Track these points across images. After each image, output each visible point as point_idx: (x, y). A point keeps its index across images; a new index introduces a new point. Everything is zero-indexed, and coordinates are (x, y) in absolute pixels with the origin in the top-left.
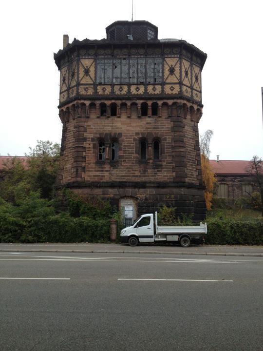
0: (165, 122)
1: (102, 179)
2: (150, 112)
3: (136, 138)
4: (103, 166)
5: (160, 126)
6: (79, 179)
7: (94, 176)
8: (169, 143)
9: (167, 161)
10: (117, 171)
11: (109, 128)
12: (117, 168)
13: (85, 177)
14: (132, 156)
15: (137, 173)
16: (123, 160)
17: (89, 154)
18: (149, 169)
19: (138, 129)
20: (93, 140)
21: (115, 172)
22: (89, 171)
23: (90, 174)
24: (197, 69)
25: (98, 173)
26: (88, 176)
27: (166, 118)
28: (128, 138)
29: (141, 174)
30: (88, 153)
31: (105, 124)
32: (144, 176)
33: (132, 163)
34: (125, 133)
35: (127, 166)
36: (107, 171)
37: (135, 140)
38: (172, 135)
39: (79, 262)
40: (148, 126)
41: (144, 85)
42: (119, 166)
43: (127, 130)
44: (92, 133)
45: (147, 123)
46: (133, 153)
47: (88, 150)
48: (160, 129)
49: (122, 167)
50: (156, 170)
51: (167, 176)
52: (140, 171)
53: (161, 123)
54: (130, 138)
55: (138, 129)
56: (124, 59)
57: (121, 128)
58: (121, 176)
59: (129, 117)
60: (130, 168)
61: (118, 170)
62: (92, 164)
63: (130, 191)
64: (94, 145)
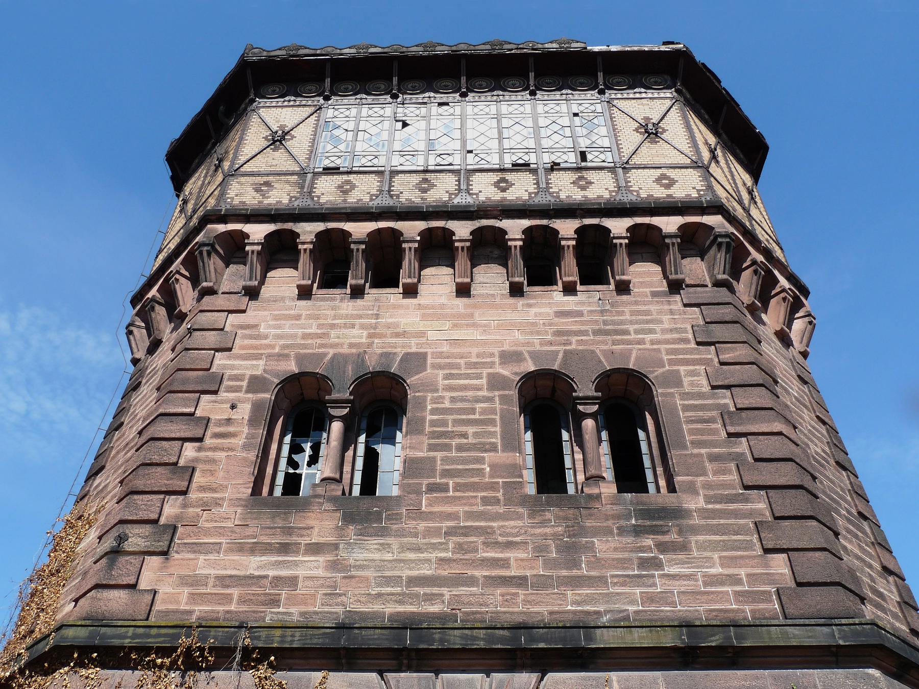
0: (653, 308)
2: (569, 269)
3: (505, 373)
4: (295, 520)
6: (115, 601)
7: (224, 581)
9: (708, 486)
10: (385, 547)
11: (358, 335)
12: (383, 532)
13: (164, 590)
14: (481, 460)
15: (519, 561)
16: (425, 482)
17: (223, 455)
18: (596, 532)
19: (518, 336)
20: (256, 384)
21: (368, 553)
22: (197, 548)
23: (205, 566)
25: (253, 564)
26: (184, 581)
28: (459, 377)
29: (548, 564)
30: (215, 449)
31: (335, 317)
32: (577, 582)
33: (486, 501)
34: (440, 355)
36: (315, 549)
37: (496, 382)
40: (568, 324)
41: (534, 171)
43: (454, 342)
44: (257, 357)
46: (493, 448)
47: (217, 436)
48: (633, 336)
49: (422, 525)
50: (649, 541)
52: (540, 550)
54: (468, 376)
55: (518, 336)
57: (422, 334)
58: (413, 581)
59: (463, 291)
60: (467, 531)
61: (389, 540)
62: (225, 509)
64: (257, 407)
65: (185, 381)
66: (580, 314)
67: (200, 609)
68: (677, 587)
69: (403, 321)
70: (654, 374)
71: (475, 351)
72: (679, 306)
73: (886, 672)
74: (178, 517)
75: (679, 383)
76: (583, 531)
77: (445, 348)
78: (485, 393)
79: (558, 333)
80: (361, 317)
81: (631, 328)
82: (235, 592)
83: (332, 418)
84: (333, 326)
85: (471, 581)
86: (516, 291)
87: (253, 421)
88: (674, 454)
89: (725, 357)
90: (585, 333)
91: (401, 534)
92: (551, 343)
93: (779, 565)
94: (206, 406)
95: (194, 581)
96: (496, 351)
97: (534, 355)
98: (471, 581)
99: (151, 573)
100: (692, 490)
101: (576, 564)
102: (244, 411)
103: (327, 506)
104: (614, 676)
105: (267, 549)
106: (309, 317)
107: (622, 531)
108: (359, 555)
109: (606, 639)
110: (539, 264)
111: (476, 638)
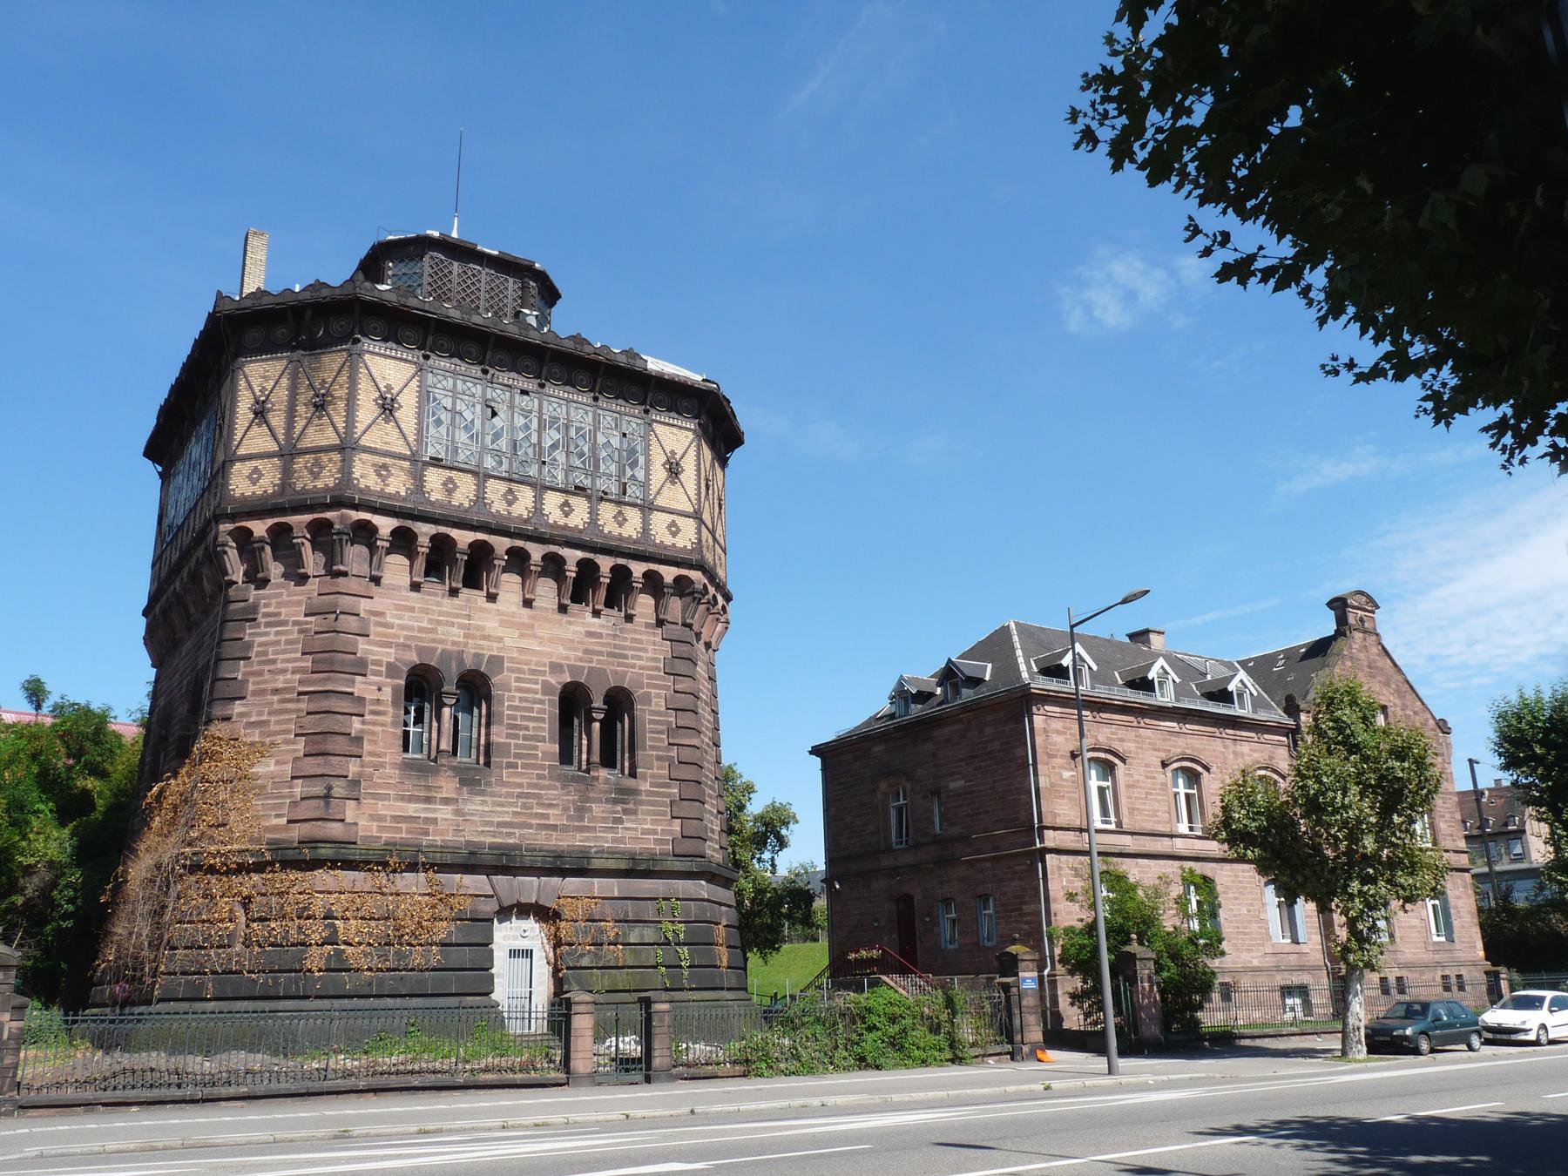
1: (427, 833)
5: (631, 649)
7: (396, 819)
8: (658, 713)
9: (653, 776)
12: (482, 793)
14: (536, 748)
15: (555, 816)
17: (379, 729)
19: (562, 650)
20: (392, 670)
21: (476, 805)
25: (412, 809)
26: (373, 818)
27: (648, 625)
29: (570, 818)
30: (374, 724)
32: (582, 829)
33: (539, 777)
34: (512, 660)
35: (520, 785)
36: (446, 801)
38: (666, 688)
39: (1394, 1078)
41: (589, 498)
42: (489, 784)
43: (522, 650)
44: (389, 645)
45: (590, 634)
50: (619, 808)
51: (655, 832)
52: (566, 809)
54: (530, 681)
55: (562, 650)
56: (524, 392)
57: (500, 639)
58: (500, 824)
60: (528, 795)
63: (531, 888)
64: (395, 689)
65: (343, 663)
66: (599, 636)
67: (386, 836)
68: (628, 834)
69: (487, 624)
70: (637, 693)
71: (535, 659)
72: (658, 639)
73: (708, 881)
74: (360, 774)
75: (649, 704)
76: (588, 800)
77: (515, 655)
78: (539, 696)
79: (587, 652)
80: (457, 616)
81: (630, 653)
82: (404, 826)
83: (445, 705)
84: (439, 622)
85: (530, 826)
86: (563, 609)
87: (395, 704)
88: (639, 753)
89: (679, 687)
91: (493, 795)
92: (581, 660)
93: (676, 826)
94: (359, 686)
95: (380, 818)
96: (547, 661)
97: (572, 669)
98: (530, 826)
99: (350, 811)
100: (644, 778)
101: (582, 819)
102: (387, 695)
103: (450, 773)
104: (596, 880)
105: (417, 799)
106: (423, 611)
107: (607, 801)
108: (470, 807)
109: (597, 864)
110: (581, 588)
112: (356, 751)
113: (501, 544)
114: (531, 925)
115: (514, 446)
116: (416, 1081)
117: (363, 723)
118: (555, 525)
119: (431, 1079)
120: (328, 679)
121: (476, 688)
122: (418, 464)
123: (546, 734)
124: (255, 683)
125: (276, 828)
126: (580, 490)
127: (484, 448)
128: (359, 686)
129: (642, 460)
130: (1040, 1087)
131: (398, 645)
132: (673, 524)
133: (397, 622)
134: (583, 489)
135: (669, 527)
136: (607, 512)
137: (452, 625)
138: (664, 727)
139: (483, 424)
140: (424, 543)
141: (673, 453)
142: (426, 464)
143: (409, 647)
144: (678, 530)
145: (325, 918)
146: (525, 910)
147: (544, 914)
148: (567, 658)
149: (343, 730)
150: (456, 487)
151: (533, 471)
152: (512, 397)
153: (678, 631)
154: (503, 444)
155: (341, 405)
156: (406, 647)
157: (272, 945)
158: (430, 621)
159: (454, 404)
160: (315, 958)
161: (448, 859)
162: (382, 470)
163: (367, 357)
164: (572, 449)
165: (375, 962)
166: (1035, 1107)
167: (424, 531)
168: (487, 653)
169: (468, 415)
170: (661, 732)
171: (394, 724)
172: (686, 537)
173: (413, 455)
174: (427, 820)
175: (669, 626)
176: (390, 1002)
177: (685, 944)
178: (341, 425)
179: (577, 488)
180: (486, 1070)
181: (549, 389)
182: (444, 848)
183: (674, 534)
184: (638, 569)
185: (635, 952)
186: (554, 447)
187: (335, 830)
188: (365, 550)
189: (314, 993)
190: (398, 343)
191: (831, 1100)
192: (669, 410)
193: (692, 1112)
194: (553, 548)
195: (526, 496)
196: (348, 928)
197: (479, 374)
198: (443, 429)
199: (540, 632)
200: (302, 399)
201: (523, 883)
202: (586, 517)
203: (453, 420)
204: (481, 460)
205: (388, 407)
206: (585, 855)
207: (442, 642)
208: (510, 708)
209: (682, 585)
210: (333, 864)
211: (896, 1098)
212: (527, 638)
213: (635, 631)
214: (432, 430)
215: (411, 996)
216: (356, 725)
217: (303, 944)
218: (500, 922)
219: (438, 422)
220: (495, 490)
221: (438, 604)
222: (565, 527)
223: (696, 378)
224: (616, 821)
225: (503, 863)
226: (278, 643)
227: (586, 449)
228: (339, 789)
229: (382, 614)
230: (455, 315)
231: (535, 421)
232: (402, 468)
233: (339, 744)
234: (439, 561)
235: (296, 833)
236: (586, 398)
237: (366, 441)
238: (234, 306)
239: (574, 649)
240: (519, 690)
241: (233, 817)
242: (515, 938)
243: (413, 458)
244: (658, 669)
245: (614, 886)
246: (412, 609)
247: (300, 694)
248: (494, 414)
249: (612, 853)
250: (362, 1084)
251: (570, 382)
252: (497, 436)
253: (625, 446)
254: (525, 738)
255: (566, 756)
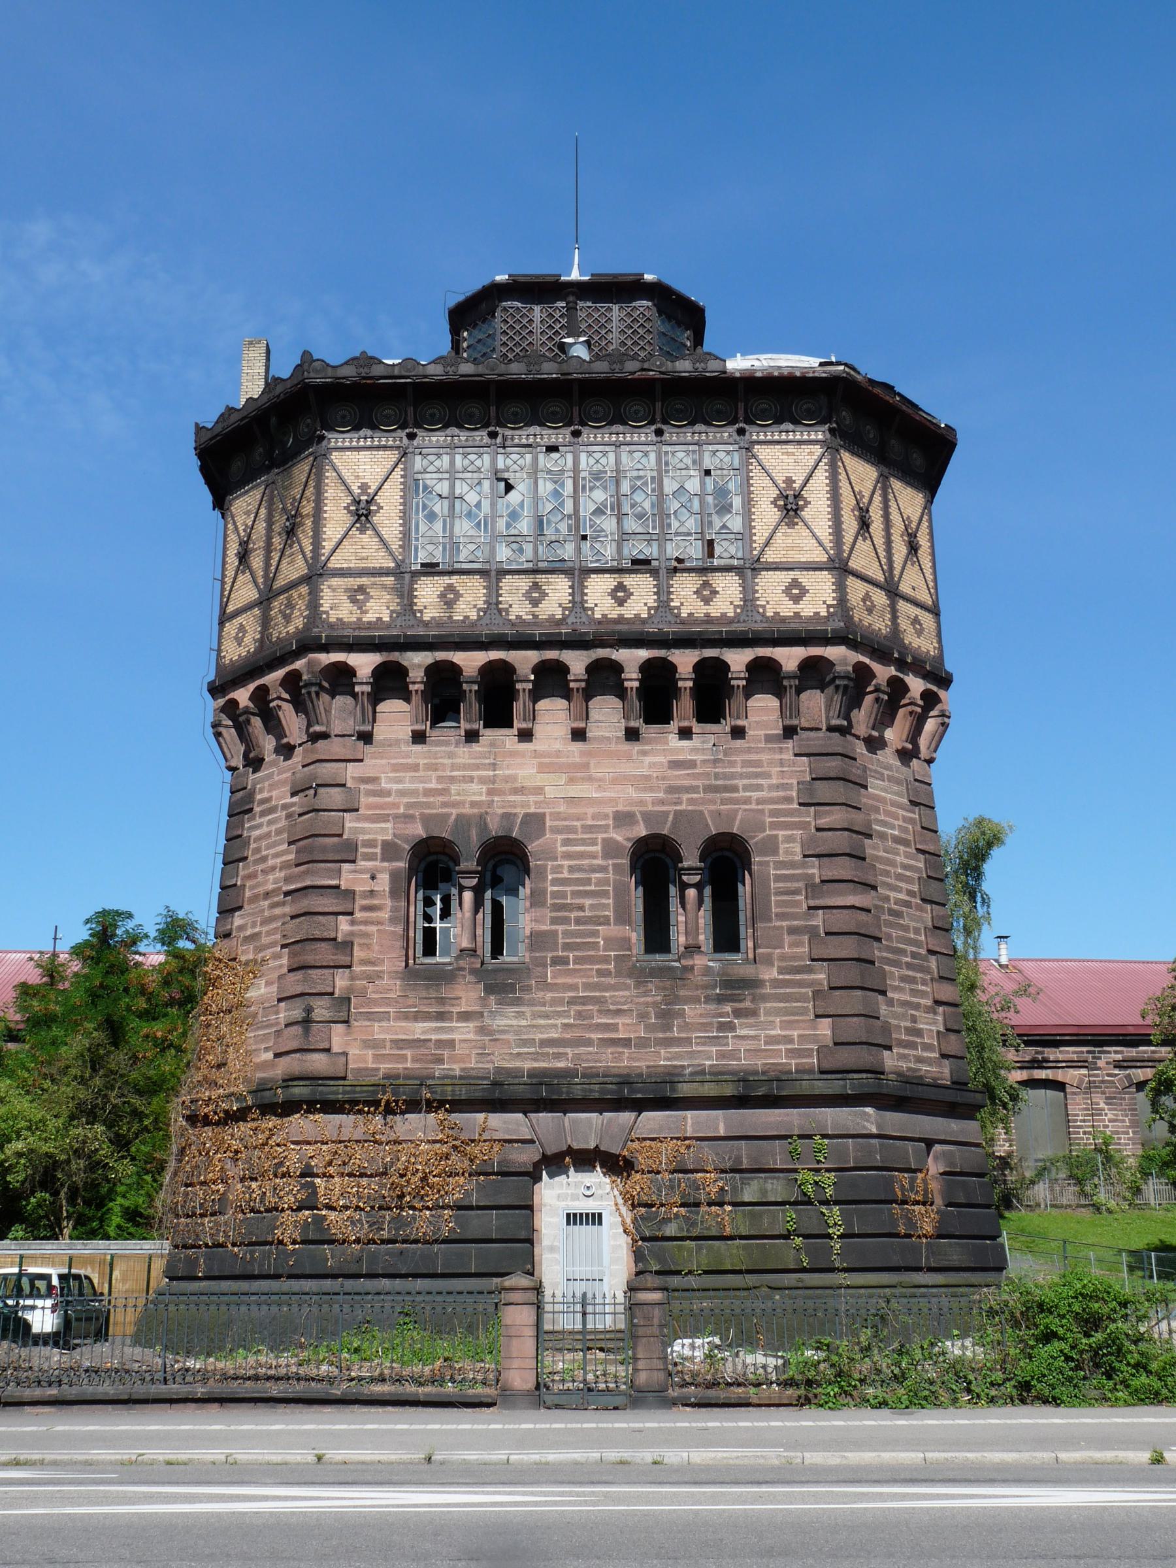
1: (440, 1060)
5: (742, 776)
7: (397, 1044)
8: (792, 865)
9: (782, 958)
12: (518, 1002)
14: (595, 934)
15: (626, 1026)
19: (632, 792)
20: (389, 850)
21: (507, 1019)
23: (380, 1031)
24: (908, 500)
25: (419, 1030)
27: (769, 739)
29: (648, 1028)
30: (366, 922)
33: (600, 973)
34: (557, 816)
35: (573, 987)
36: (465, 1016)
38: (804, 826)
39: (218, 1515)
40: (680, 777)
41: (655, 573)
42: (527, 989)
43: (571, 801)
44: (384, 818)
45: (676, 764)
50: (728, 1008)
52: (643, 1016)
53: (746, 763)
54: (583, 842)
55: (632, 792)
56: (552, 449)
57: (539, 790)
58: (544, 1043)
60: (585, 1001)
63: (588, 1128)
64: (394, 876)
65: (324, 849)
66: (692, 764)
67: (385, 1067)
68: (743, 1046)
69: (521, 773)
70: (755, 840)
71: (590, 811)
72: (788, 756)
73: (879, 1107)
74: (350, 989)
75: (775, 852)
76: (677, 1000)
78: (599, 862)
79: (671, 790)
80: (477, 767)
81: (740, 783)
82: (408, 1053)
84: (452, 779)
85: (588, 1042)
86: (632, 735)
87: (394, 893)
89: (823, 822)
90: (694, 789)
91: (532, 1003)
93: (825, 1029)
94: (349, 876)
96: (609, 811)
97: (648, 817)
98: (588, 1042)
99: (338, 1038)
100: (768, 961)
101: (668, 1028)
102: (383, 883)
103: (470, 978)
104: (689, 1114)
107: (708, 999)
108: (500, 1022)
109: (685, 1090)
110: (655, 700)
111: (591, 1091)
112: (344, 959)
113: (525, 661)
114: (597, 1179)
115: (539, 522)
116: (275, 1390)
117: (353, 923)
118: (605, 620)
119: (298, 1388)
120: (307, 872)
121: (505, 860)
122: (404, 577)
123: (610, 913)
124: (252, 888)
125: (264, 1065)
126: (641, 565)
127: (496, 537)
128: (349, 876)
129: (737, 502)
130: (1145, 1456)
131: (396, 817)
132: (795, 583)
133: (395, 786)
134: (647, 562)
135: (787, 591)
136: (684, 589)
137: (471, 779)
138: (801, 885)
139: (493, 505)
140: (417, 675)
141: (789, 481)
142: (415, 574)
143: (412, 817)
144: (804, 591)
145: (303, 1175)
146: (585, 1159)
147: (617, 1165)
148: (642, 803)
149: (326, 935)
150: (458, 595)
151: (568, 551)
152: (535, 460)
153: (820, 740)
154: (524, 526)
155: (309, 523)
156: (408, 818)
157: (252, 1211)
158: (440, 779)
159: (452, 487)
160: (288, 1226)
161: (463, 1093)
162: (358, 596)
163: (335, 456)
164: (626, 508)
165: (364, 1231)
166: (739, 1499)
167: (417, 662)
168: (521, 811)
169: (472, 498)
170: (796, 892)
171: (393, 920)
172: (820, 595)
173: (398, 566)
174: (440, 1043)
175: (805, 735)
176: (385, 1283)
177: (836, 1203)
178: (308, 548)
179: (635, 562)
180: (382, 1379)
181: (588, 435)
182: (466, 1079)
183: (797, 599)
184: (738, 660)
185: (753, 1215)
186: (599, 511)
187: (317, 1063)
188: (349, 700)
189: (286, 1271)
190: (374, 427)
191: (243, 1455)
192: (778, 421)
193: (429, 1460)
194: (602, 653)
195: (559, 590)
196: (328, 1188)
197: (486, 440)
198: (438, 526)
199: (596, 772)
200: (277, 528)
201: (573, 1122)
202: (652, 601)
203: (452, 507)
204: (493, 551)
205: (363, 513)
206: (671, 1077)
207: (455, 804)
208: (555, 882)
209: (814, 673)
210: (311, 1106)
211: (814, 1458)
212: (586, 783)
213: (749, 750)
214: (423, 528)
215: (416, 1276)
216: (344, 925)
217: (276, 1209)
218: (551, 1176)
219: (431, 517)
220: (514, 590)
221: (451, 755)
222: (621, 620)
223: (804, 362)
224: (722, 1027)
225: (545, 1095)
226: (268, 835)
227: (647, 505)
228: (321, 1010)
229: (374, 780)
230: (517, 370)
231: (569, 484)
232: (384, 587)
233: (323, 953)
234: (443, 698)
235: (283, 1067)
236: (646, 435)
237: (336, 563)
238: (209, 435)
239: (651, 789)
240: (568, 856)
241: (231, 1054)
242: (575, 1197)
243: (398, 572)
244: (788, 800)
245: (719, 1121)
246: (415, 768)
247: (287, 894)
248: (509, 488)
249: (717, 1075)
250: (200, 1390)
251: (618, 419)
252: (514, 516)
253: (710, 488)
254: (578, 921)
255: (657, 935)
